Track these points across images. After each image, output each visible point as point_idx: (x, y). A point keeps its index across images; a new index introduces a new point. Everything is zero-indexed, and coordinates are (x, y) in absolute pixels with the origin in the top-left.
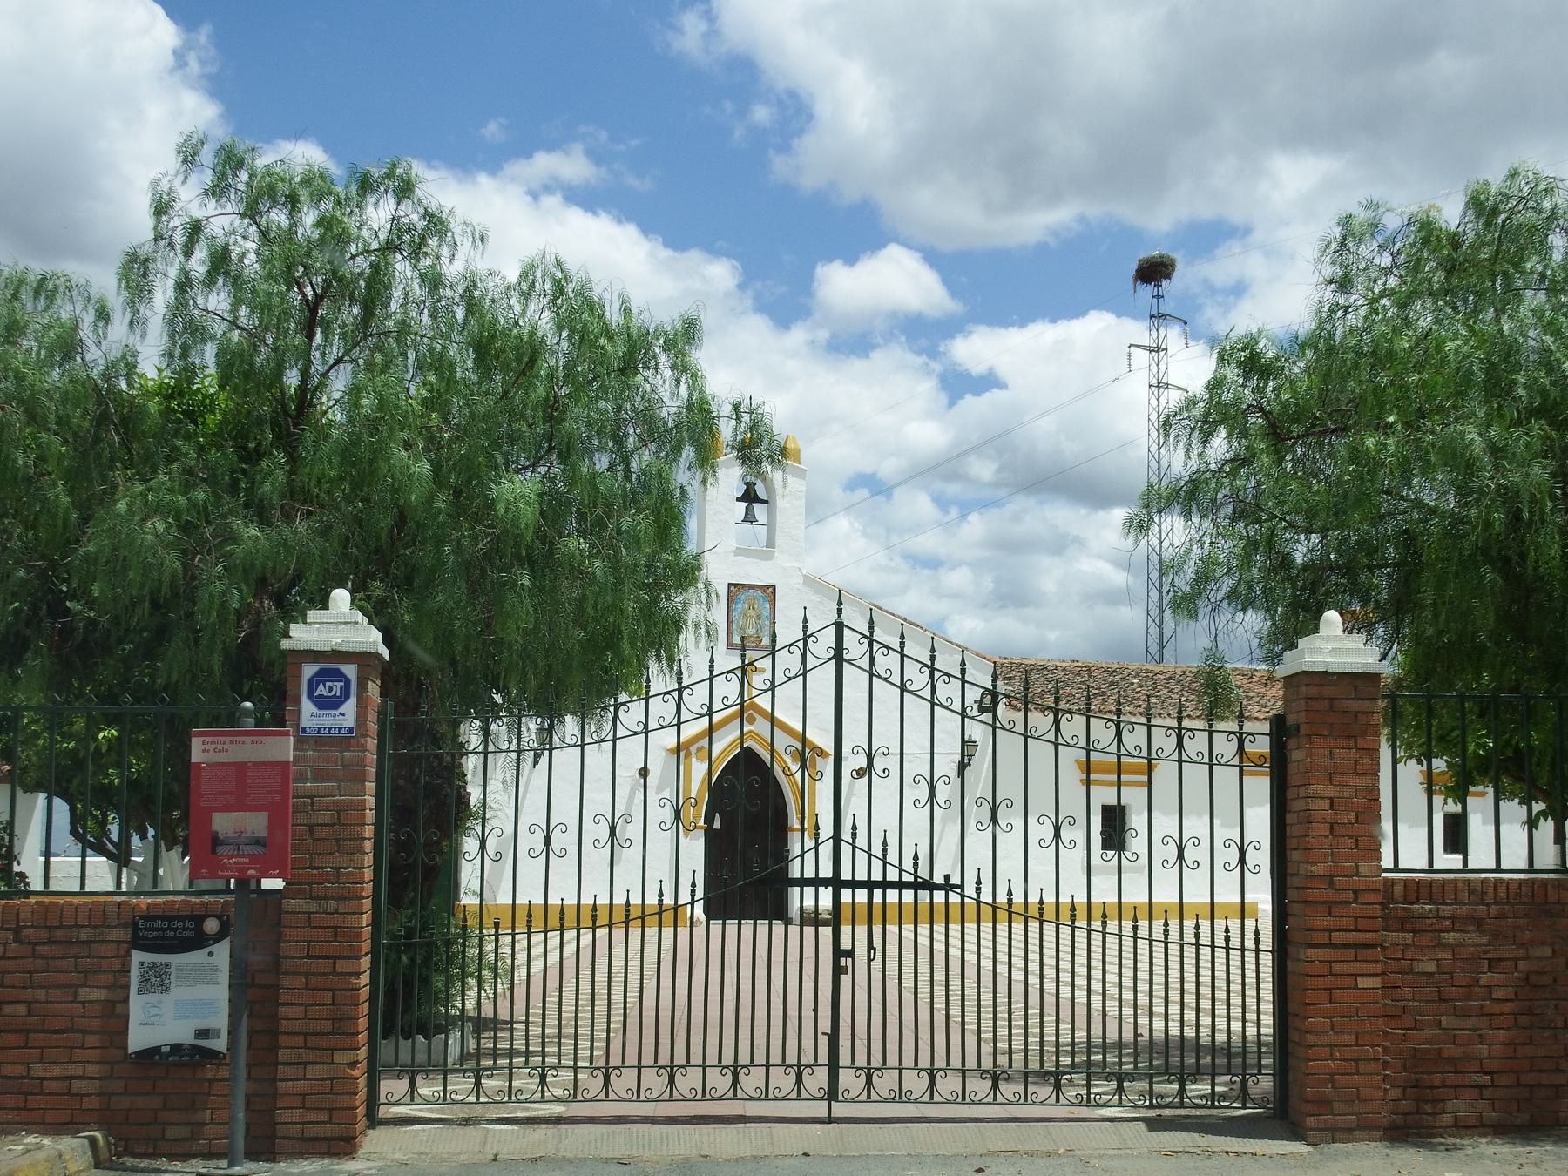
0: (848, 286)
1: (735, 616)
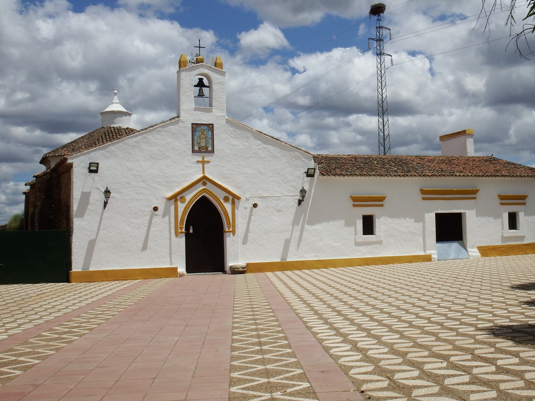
0: (251, 39)
1: (196, 138)
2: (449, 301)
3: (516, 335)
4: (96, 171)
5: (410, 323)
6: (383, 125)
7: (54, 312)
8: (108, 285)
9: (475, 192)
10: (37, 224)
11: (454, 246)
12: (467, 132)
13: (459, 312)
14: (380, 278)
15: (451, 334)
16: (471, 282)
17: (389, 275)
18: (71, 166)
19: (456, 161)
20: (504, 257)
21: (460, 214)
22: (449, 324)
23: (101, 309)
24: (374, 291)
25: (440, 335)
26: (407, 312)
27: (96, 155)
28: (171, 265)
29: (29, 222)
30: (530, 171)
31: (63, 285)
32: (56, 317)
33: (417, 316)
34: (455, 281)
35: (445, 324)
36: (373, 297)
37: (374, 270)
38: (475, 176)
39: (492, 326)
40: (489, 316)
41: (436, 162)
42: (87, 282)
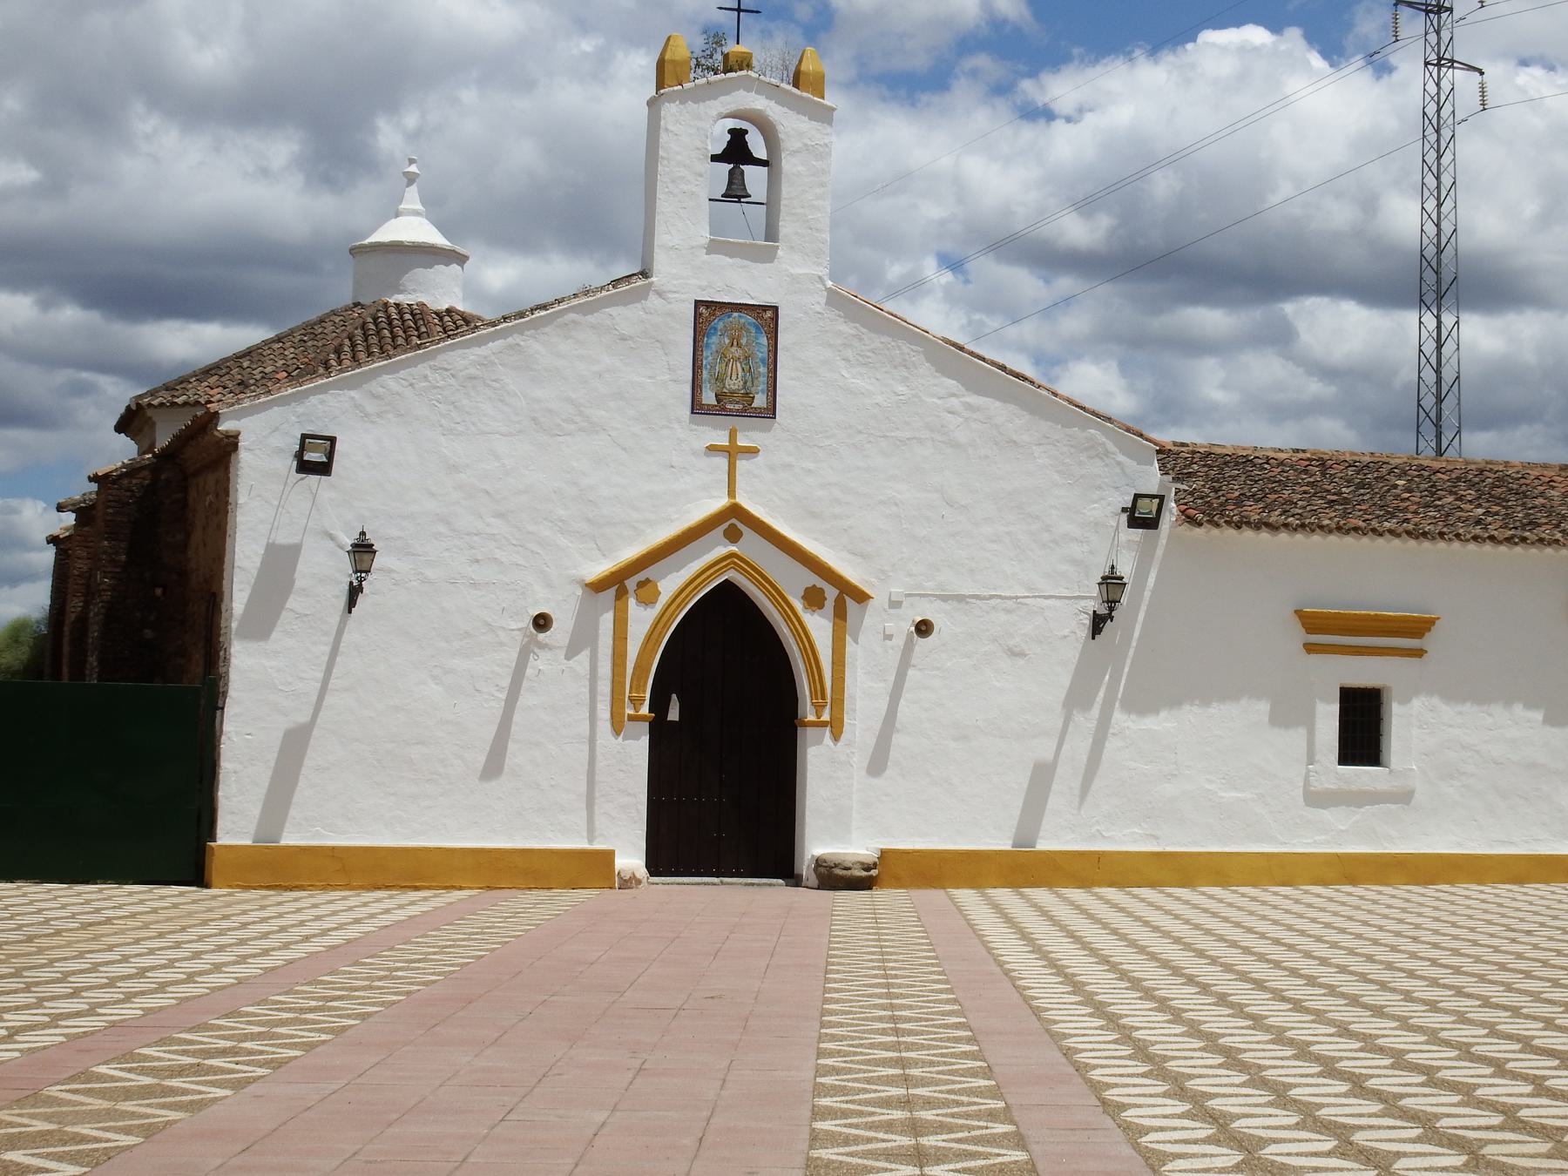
1: (708, 356)
4: (324, 469)
7: (142, 993)
8: (280, 899)
10: (93, 660)
17: (1436, 925)
18: (230, 444)
23: (319, 990)
24: (1372, 981)
27: (327, 405)
29: (66, 649)
31: (181, 894)
32: (148, 1011)
36: (1365, 1006)
37: (1375, 902)
42: (268, 888)
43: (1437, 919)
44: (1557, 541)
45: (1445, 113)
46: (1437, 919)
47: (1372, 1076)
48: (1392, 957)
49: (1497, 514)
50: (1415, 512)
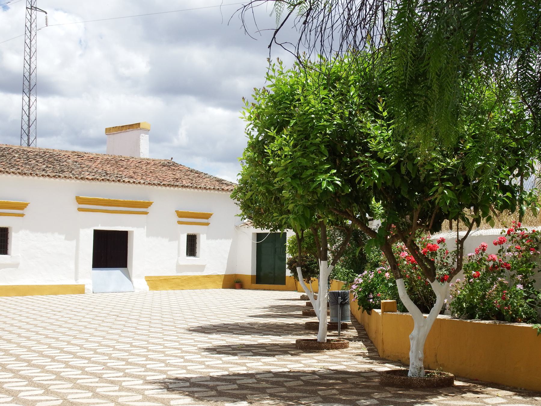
2: (109, 346)
3: (195, 389)
5: (57, 374)
6: (29, 106)
9: (147, 205)
11: (116, 273)
12: (141, 126)
13: (123, 360)
14: (14, 314)
15: (112, 389)
16: (136, 321)
17: (27, 310)
19: (125, 163)
20: (178, 292)
21: (126, 233)
22: (109, 375)
24: (6, 331)
25: (98, 390)
26: (53, 359)
28: (76, 280)
30: (217, 183)
33: (67, 365)
34: (116, 320)
35: (104, 376)
36: (4, 340)
37: (5, 303)
38: (149, 183)
39: (164, 379)
40: (160, 366)
41: (99, 161)
43: (28, 308)
44: (71, 177)
45: (33, 26)
46: (28, 308)
47: (9, 364)
48: (13, 322)
49: (50, 167)
50: (22, 166)
